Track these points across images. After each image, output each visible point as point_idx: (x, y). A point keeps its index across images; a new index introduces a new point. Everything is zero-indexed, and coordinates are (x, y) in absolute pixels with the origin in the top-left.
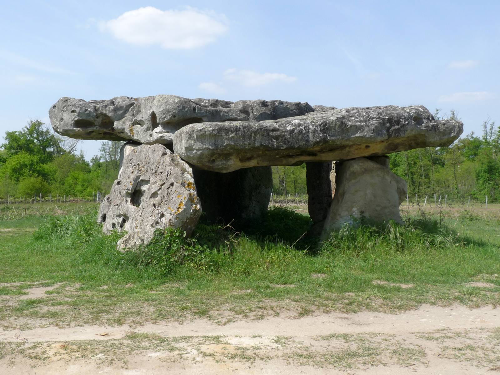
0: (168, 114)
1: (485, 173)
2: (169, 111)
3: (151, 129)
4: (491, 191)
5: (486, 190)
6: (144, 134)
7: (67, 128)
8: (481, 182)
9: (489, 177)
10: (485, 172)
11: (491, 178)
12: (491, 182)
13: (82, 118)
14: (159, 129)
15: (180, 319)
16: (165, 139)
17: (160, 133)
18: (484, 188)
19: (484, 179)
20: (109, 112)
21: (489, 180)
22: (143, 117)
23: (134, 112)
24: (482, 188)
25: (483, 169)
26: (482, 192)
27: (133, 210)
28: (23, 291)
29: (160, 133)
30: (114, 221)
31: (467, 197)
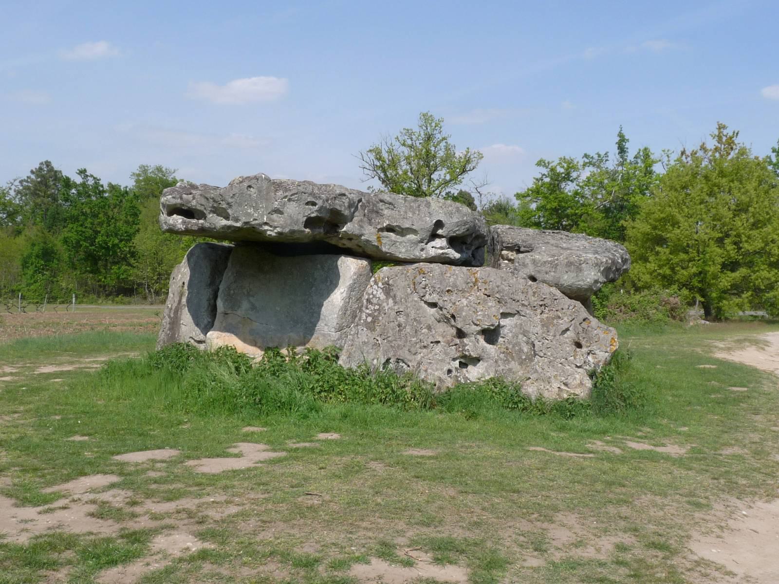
0: (463, 227)
1: (38, 259)
2: (466, 223)
3: (425, 241)
4: (47, 285)
5: (38, 284)
6: (411, 247)
7: (296, 228)
8: (30, 272)
9: (43, 265)
10: (37, 256)
11: (46, 266)
12: (47, 273)
13: (321, 215)
14: (440, 243)
15: (644, 450)
16: (448, 257)
17: (442, 248)
18: (35, 282)
19: (36, 267)
20: (341, 206)
21: (43, 269)
22: (413, 225)
23: (366, 211)
24: (32, 281)
25: (34, 252)
26: (32, 287)
27: (493, 350)
28: (43, 557)
29: (442, 248)
30: (450, 367)
31: (4, 295)
